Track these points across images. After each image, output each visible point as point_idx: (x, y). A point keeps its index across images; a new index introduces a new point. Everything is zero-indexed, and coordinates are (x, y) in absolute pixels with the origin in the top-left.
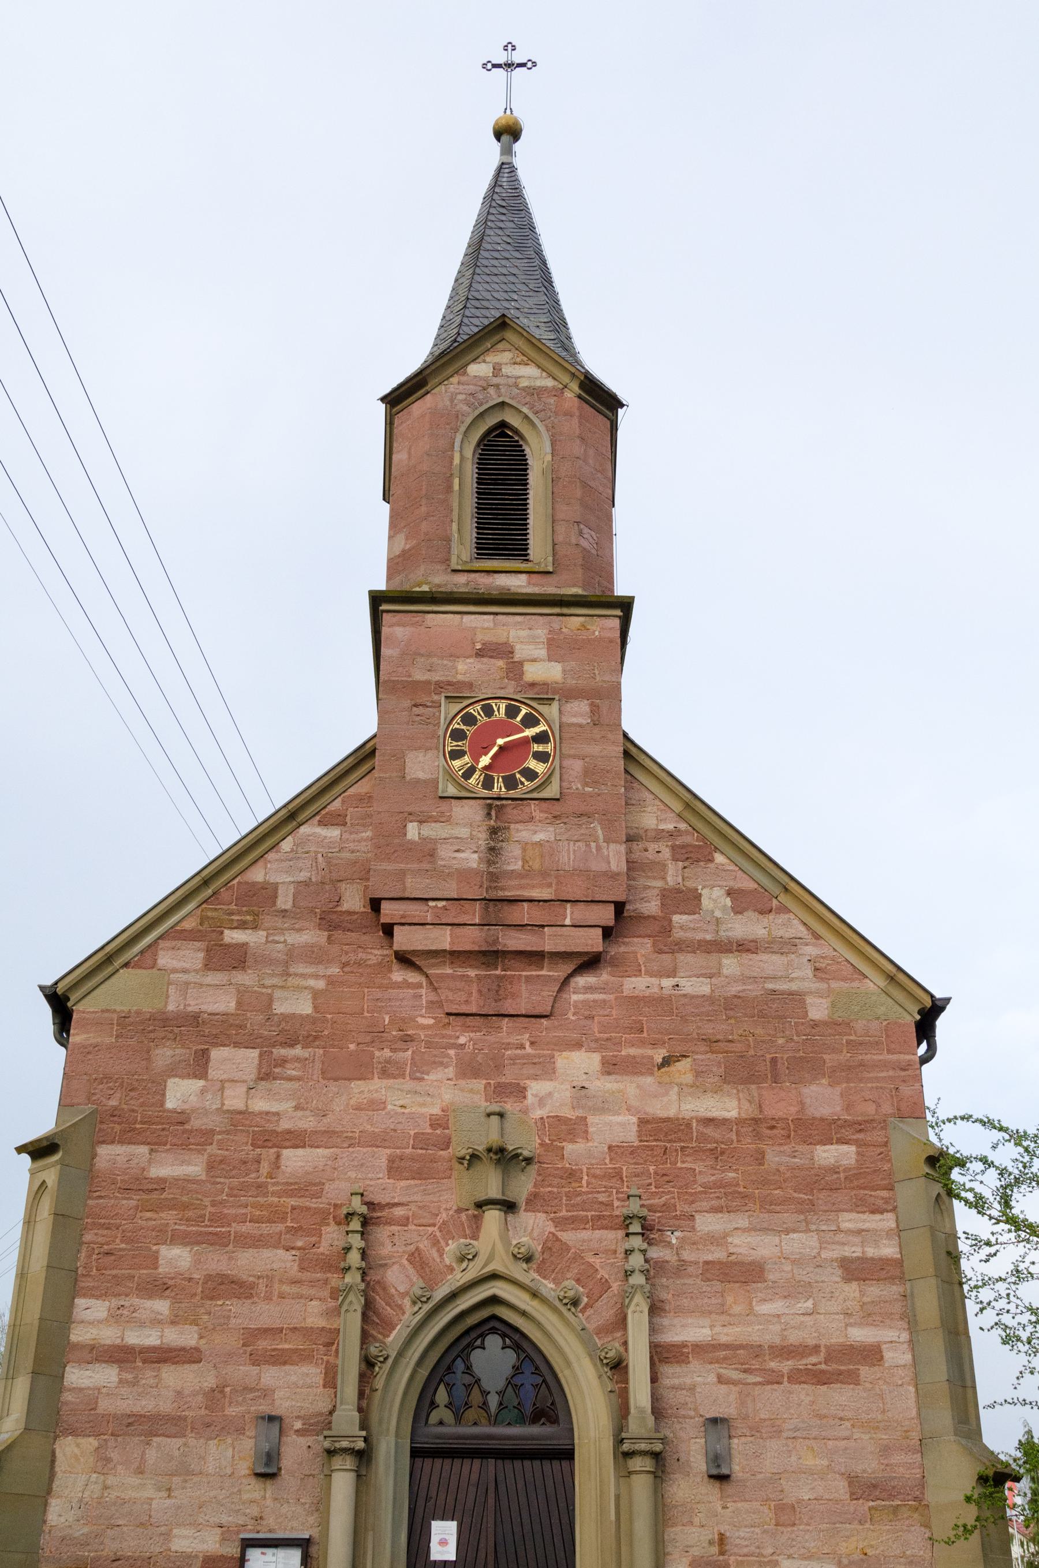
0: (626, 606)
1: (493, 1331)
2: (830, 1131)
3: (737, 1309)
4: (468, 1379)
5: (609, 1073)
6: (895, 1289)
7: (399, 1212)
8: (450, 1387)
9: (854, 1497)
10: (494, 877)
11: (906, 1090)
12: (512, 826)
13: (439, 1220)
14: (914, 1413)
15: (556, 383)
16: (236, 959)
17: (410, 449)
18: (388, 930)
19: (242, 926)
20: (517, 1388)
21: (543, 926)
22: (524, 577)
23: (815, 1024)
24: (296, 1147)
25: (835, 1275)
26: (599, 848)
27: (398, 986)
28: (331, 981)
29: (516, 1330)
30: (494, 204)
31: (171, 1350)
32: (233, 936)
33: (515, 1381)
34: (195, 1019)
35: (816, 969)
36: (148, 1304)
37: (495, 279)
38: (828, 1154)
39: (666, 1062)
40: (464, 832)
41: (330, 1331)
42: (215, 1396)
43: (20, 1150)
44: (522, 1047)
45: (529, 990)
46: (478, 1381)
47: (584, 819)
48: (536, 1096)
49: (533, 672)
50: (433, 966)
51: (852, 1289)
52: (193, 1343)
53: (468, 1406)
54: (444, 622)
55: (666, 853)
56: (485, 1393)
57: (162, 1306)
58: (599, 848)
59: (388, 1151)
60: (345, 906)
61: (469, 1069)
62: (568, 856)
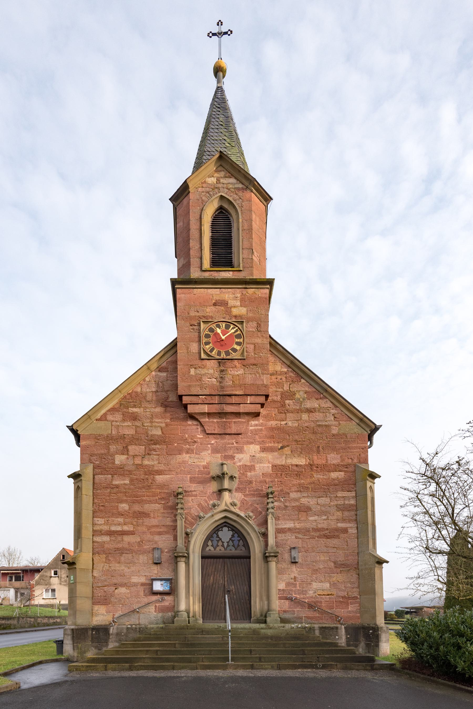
0: (270, 283)
1: (225, 526)
2: (336, 468)
3: (302, 519)
4: (218, 539)
5: (263, 452)
6: (353, 513)
7: (194, 493)
8: (212, 541)
9: (336, 567)
10: (222, 387)
11: (363, 455)
12: (229, 369)
13: (207, 495)
14: (356, 546)
15: (243, 186)
16: (134, 417)
17: (183, 220)
18: (185, 406)
19: (135, 406)
20: (233, 541)
21: (240, 404)
22: (231, 273)
23: (334, 435)
24: (159, 475)
25: (333, 510)
26: (260, 376)
27: (189, 425)
28: (167, 425)
29: (232, 526)
30: (214, 107)
31: (125, 531)
32: (132, 410)
33: (232, 539)
34: (123, 437)
35: (335, 417)
36: (116, 519)
37: (216, 142)
38: (334, 475)
39: (282, 448)
40: (211, 371)
41: (174, 526)
42: (140, 544)
43: (69, 477)
44: (233, 444)
45: (234, 425)
46: (221, 539)
47: (255, 366)
48: (238, 459)
49: (235, 311)
50: (202, 418)
51: (340, 514)
52: (132, 530)
53: (218, 546)
54: (200, 292)
55: (284, 379)
56: (223, 542)
57: (121, 520)
58: (260, 376)
59: (189, 476)
60: (170, 399)
61: (215, 451)
62: (249, 379)
